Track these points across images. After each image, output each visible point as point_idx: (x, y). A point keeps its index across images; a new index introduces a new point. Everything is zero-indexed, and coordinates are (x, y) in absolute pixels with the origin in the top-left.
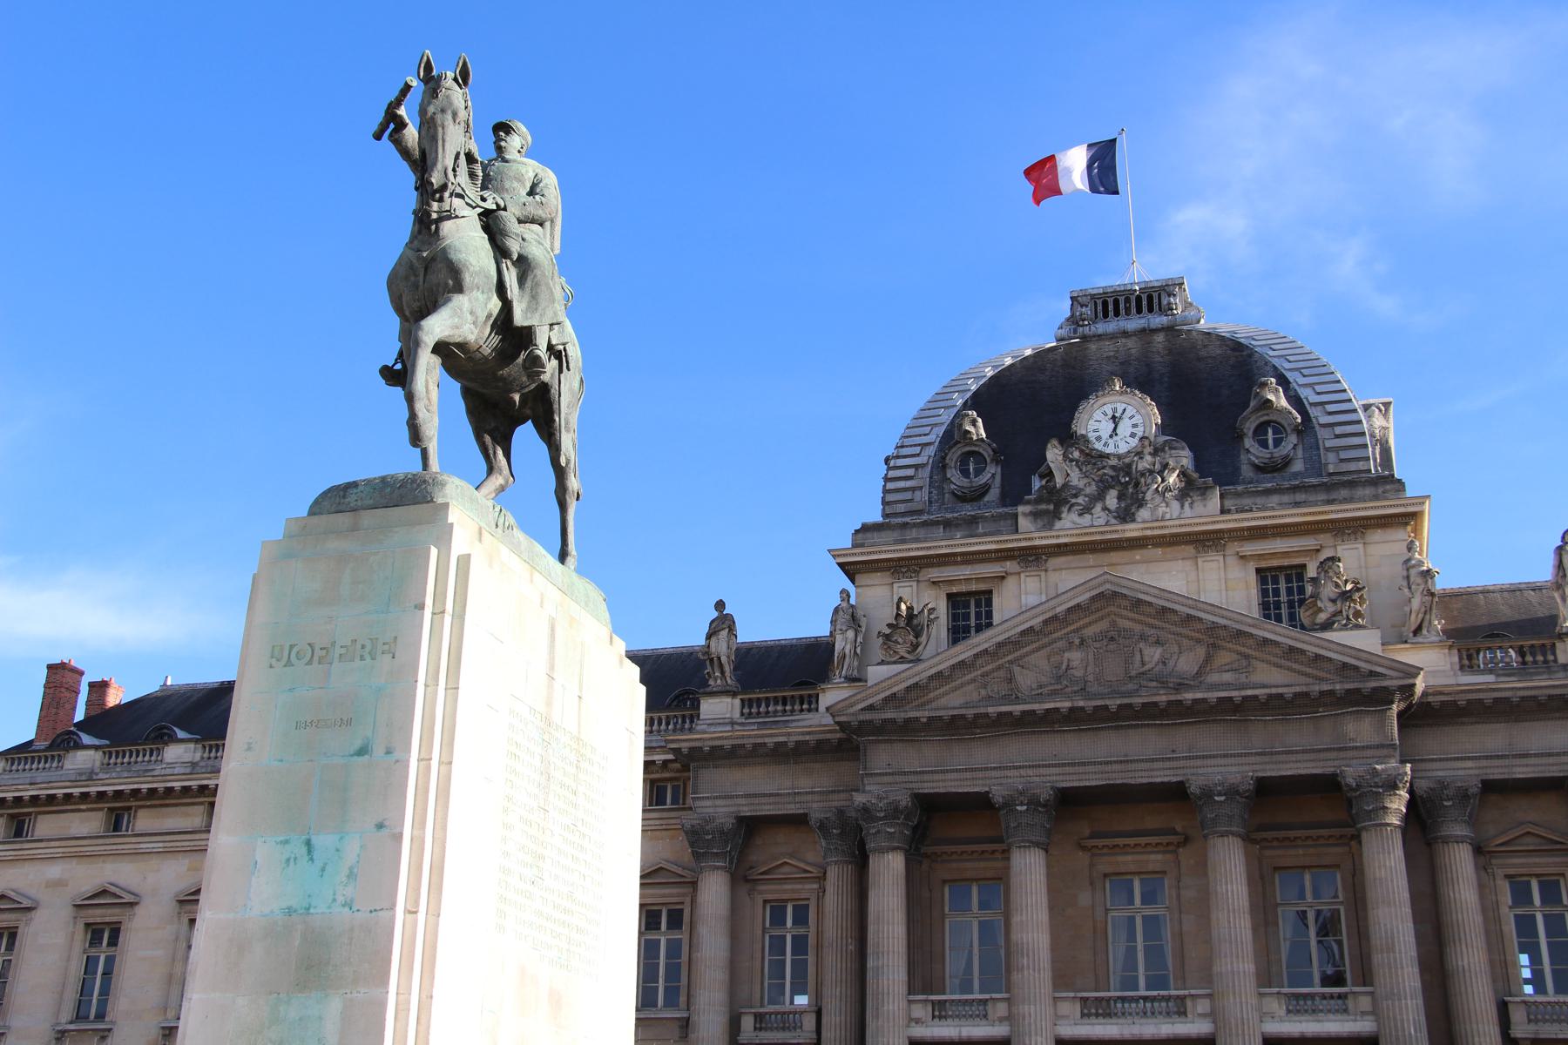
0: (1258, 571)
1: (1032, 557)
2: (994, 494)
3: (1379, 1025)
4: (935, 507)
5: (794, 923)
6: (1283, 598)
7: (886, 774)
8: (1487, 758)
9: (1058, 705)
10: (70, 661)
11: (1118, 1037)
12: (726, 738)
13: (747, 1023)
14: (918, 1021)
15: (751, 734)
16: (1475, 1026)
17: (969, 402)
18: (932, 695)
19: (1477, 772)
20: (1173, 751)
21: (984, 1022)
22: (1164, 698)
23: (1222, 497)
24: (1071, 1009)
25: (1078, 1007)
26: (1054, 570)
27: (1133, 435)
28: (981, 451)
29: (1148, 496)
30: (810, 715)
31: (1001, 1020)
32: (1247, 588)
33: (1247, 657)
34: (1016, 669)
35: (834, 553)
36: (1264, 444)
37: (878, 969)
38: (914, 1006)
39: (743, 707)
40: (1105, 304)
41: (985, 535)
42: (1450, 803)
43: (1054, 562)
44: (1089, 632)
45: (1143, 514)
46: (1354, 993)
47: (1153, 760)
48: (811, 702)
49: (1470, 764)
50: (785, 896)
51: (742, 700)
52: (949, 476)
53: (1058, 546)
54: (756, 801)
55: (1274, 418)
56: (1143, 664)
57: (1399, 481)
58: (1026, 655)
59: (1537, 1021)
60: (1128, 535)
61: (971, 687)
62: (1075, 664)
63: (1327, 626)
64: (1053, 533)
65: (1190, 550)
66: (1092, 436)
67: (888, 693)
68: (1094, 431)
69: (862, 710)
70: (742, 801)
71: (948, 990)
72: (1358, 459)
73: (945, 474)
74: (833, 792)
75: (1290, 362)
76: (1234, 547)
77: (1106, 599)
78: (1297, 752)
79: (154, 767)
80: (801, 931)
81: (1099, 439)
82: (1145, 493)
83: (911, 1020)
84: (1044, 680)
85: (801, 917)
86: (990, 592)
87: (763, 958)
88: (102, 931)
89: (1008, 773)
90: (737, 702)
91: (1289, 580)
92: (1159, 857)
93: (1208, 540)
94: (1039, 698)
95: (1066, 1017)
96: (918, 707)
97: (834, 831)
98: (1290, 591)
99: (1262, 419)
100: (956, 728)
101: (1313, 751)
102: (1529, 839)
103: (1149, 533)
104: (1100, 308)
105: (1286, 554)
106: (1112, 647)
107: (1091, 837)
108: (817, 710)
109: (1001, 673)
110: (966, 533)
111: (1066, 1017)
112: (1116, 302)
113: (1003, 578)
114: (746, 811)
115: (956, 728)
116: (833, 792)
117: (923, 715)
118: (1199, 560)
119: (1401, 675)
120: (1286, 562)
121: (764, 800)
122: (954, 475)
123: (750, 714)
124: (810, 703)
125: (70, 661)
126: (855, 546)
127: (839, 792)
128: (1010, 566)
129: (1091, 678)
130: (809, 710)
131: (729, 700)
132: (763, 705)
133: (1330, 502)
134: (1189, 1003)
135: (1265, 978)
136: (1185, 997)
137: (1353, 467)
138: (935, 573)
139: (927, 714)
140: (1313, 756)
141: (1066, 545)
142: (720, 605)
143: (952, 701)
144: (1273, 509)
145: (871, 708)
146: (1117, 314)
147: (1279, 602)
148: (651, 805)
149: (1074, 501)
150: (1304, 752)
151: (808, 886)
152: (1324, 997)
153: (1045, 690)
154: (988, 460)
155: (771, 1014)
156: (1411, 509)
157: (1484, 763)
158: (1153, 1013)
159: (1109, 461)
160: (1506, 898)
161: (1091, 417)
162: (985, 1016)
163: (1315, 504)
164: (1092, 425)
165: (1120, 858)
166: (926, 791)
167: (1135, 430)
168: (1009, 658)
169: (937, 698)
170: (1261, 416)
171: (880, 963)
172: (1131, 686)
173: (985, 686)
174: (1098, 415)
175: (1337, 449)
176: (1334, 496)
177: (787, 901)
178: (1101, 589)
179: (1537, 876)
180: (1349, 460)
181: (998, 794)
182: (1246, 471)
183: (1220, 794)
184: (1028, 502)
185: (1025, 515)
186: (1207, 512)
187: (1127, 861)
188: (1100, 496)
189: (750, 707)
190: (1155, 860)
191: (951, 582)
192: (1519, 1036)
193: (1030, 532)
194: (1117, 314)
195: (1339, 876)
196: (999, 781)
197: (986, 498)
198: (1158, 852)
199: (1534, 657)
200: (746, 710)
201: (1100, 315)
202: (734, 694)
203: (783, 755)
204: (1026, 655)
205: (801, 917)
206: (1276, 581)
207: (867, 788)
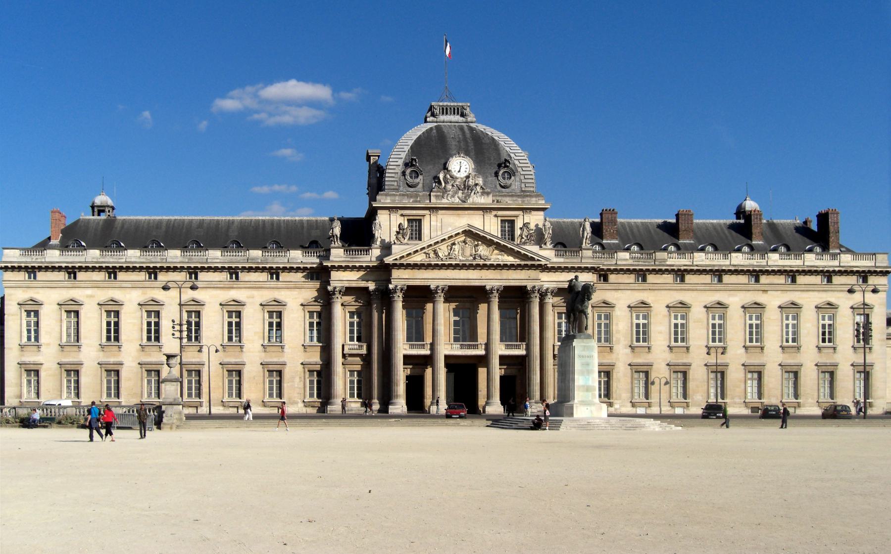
1: (434, 209)
2: (420, 185)
10: (702, 409)
13: (346, 348)
22: (482, 263)
23: (493, 196)
24: (503, 347)
27: (466, 171)
40: (443, 109)
43: (440, 212)
49: (555, 283)
52: (406, 178)
54: (351, 282)
63: (525, 243)
66: (453, 170)
67: (402, 255)
68: (454, 168)
71: (461, 340)
75: (516, 156)
76: (494, 213)
79: (122, 257)
81: (455, 171)
104: (441, 111)
112: (447, 109)
114: (347, 285)
122: (408, 177)
125: (702, 409)
145: (396, 259)
146: (447, 114)
149: (448, 193)
157: (559, 283)
159: (550, 243)
160: (556, 318)
167: (466, 170)
174: (455, 163)
184: (434, 192)
188: (456, 193)
194: (447, 114)
197: (418, 187)
201: (441, 113)
207: (392, 283)
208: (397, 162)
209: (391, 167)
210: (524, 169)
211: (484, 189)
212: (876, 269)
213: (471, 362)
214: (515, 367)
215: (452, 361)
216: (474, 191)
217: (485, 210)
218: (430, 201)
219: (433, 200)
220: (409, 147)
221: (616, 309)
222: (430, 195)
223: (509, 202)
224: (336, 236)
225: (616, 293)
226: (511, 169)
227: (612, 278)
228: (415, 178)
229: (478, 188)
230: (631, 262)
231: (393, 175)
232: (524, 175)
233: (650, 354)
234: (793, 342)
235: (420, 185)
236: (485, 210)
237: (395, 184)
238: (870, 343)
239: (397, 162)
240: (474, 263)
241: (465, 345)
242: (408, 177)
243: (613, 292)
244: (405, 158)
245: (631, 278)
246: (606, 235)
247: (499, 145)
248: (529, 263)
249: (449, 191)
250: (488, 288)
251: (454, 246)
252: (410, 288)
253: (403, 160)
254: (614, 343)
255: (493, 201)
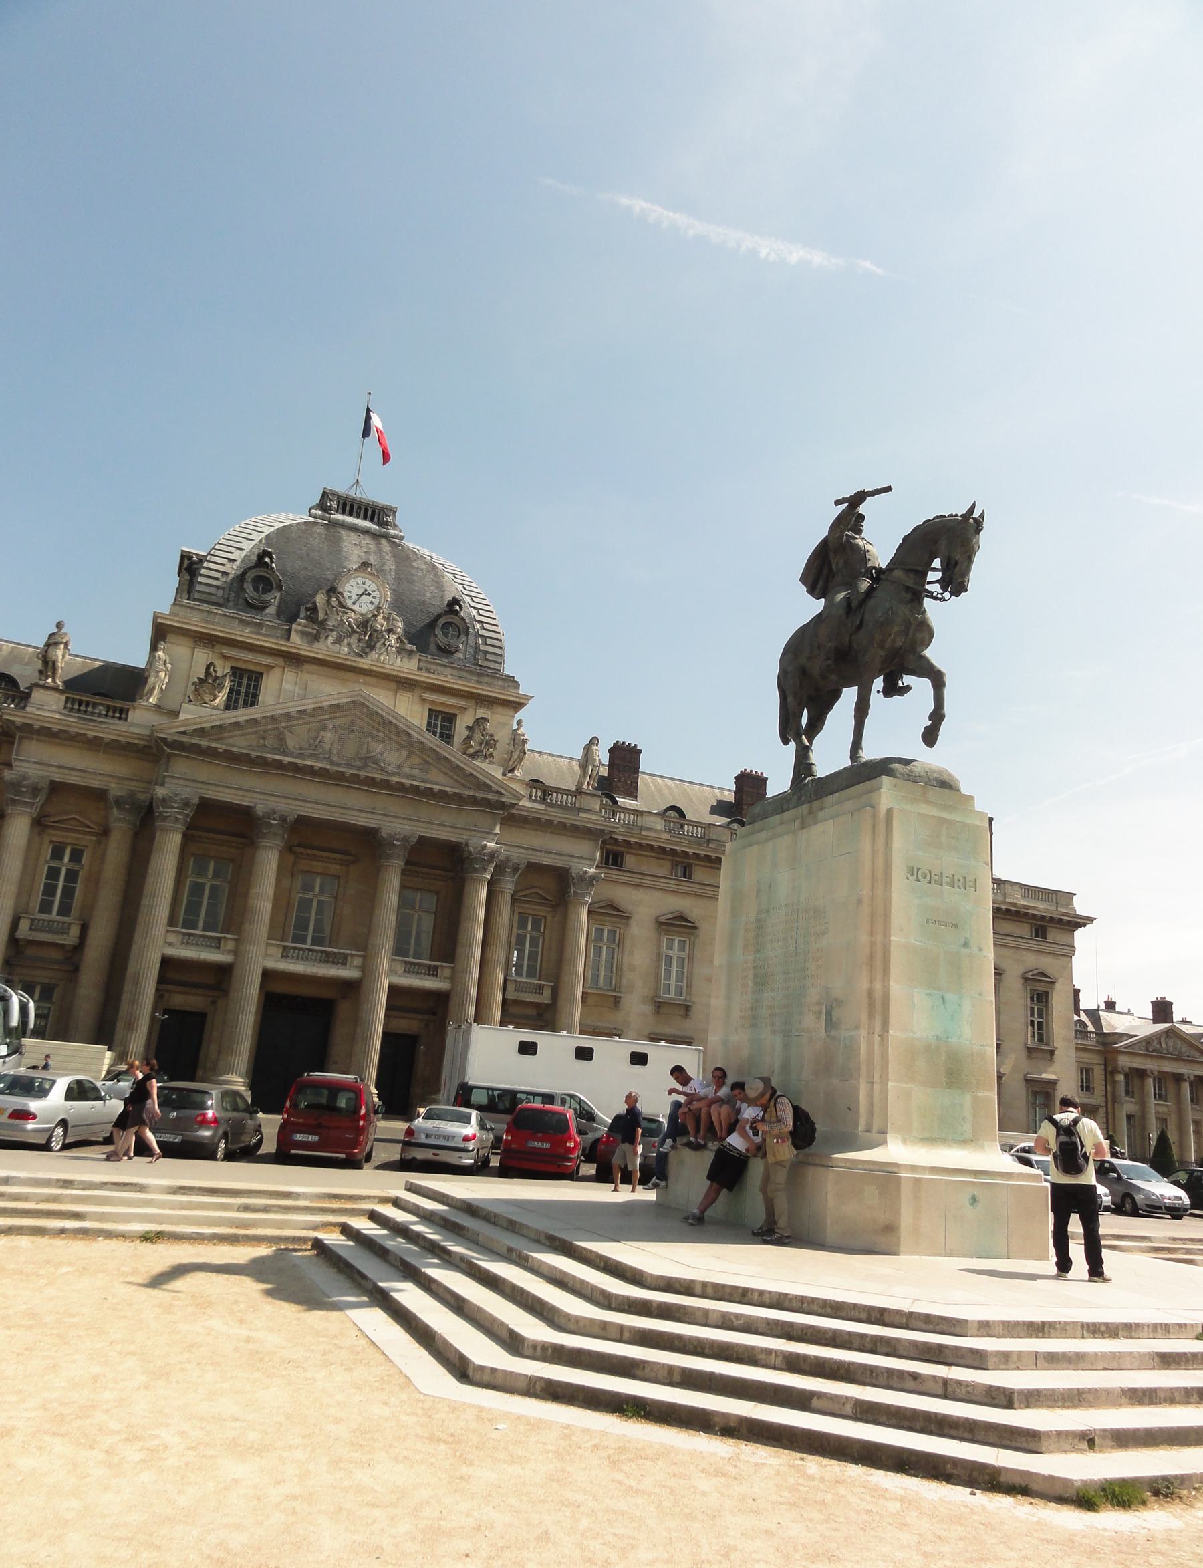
0: (430, 710)
1: (295, 660)
2: (271, 610)
3: (235, 959)
4: (231, 604)
5: (70, 860)
6: (243, 689)
7: (182, 779)
8: (532, 849)
9: (313, 764)
11: (302, 973)
12: (54, 723)
13: (24, 925)
14: (170, 944)
15: (73, 723)
16: (149, 954)
17: (263, 540)
18: (226, 735)
19: (525, 856)
20: (374, 809)
21: (216, 951)
22: (380, 776)
24: (400, 969)
25: (280, 951)
26: (308, 672)
28: (271, 578)
29: (378, 645)
30: (121, 722)
31: (229, 952)
32: (422, 718)
33: (429, 763)
34: (287, 734)
35: (156, 617)
36: (446, 635)
37: (152, 907)
38: (169, 934)
39: (66, 702)
41: (265, 635)
42: (25, 789)
43: (307, 667)
44: (338, 722)
45: (374, 655)
46: (352, 955)
47: (361, 811)
48: (123, 714)
49: (523, 851)
50: (68, 841)
51: (67, 698)
53: (314, 658)
54: (67, 772)
55: (456, 622)
56: (368, 751)
57: (517, 682)
58: (295, 725)
59: (518, 990)
60: (361, 666)
61: (253, 736)
62: (326, 740)
64: (288, 644)
65: (393, 685)
66: (346, 594)
67: (199, 726)
69: (178, 732)
70: (54, 769)
71: (219, 929)
72: (496, 662)
73: (243, 585)
74: (128, 779)
76: (418, 692)
77: (357, 706)
78: (445, 826)
80: (75, 867)
81: (350, 597)
82: (376, 643)
83: (165, 942)
84: (304, 745)
85: (76, 856)
86: (261, 674)
87: (543, 949)
88: (64, 850)
89: (268, 798)
90: (63, 698)
91: (250, 679)
92: (338, 867)
93: (406, 684)
94: (301, 756)
95: (272, 956)
96: (216, 740)
97: (127, 806)
98: (248, 686)
99: (449, 620)
100: (233, 758)
101: (452, 827)
102: (72, 823)
103: (374, 668)
105: (448, 706)
106: (351, 736)
107: (297, 846)
108: (126, 719)
109: (276, 732)
110: (255, 630)
111: (272, 956)
113: (273, 667)
114: (57, 777)
115: (233, 758)
116: (128, 779)
117: (221, 747)
118: (286, 670)
119: (512, 797)
120: (446, 710)
121: (73, 773)
122: (248, 587)
123: (71, 710)
124: (121, 713)
126: (172, 613)
127: (133, 780)
128: (280, 661)
129: (335, 752)
130: (120, 718)
131: (57, 695)
132: (84, 706)
133: (478, 682)
134: (349, 958)
135: (172, 922)
136: (348, 954)
137: (492, 665)
138: (227, 651)
139: (224, 747)
140: (452, 830)
141: (319, 659)
142: (59, 625)
143: (239, 744)
144: (446, 676)
145: (184, 733)
147: (240, 691)
148: (602, 863)
150: (449, 826)
151: (90, 838)
152: (202, 936)
153: (306, 752)
154: (274, 586)
155: (39, 920)
156: (522, 701)
158: (303, 959)
161: (348, 582)
162: (218, 948)
163: (469, 681)
164: (347, 587)
165: (315, 863)
166: (352, 822)
168: (283, 724)
169: (232, 737)
170: (261, 571)
171: (155, 903)
172: (358, 763)
173: (264, 738)
175: (485, 652)
176: (481, 680)
177: (67, 844)
178: (355, 699)
179: (533, 915)
180: (491, 661)
181: (260, 810)
182: (433, 648)
183: (397, 840)
185: (296, 631)
186: (407, 667)
187: (317, 866)
189: (73, 704)
190: (335, 868)
191: (236, 660)
192: (509, 997)
193: (297, 643)
195: (231, 865)
196: (261, 801)
197: (268, 610)
198: (337, 864)
199: (121, 715)
200: (69, 705)
202: (62, 692)
203: (94, 744)
204: (295, 725)
205: (76, 856)
206: (436, 719)
208: (231, 553)
209: (211, 566)
210: (488, 641)
211: (404, 643)
212: (1062, 917)
213: (325, 993)
214: (420, 1017)
215: (281, 988)
216: (383, 640)
217: (404, 684)
218: (288, 639)
219: (295, 638)
220: (263, 535)
221: (633, 923)
222: (289, 631)
223: (446, 677)
224: (54, 663)
225: (634, 892)
226: (463, 619)
227: (630, 861)
228: (263, 593)
229: (393, 639)
230: (666, 836)
231: (218, 575)
232: (481, 622)
233: (688, 1020)
234: (528, 976)
235: (271, 610)
236: (404, 684)
237: (220, 593)
238: (1051, 1044)
239: (231, 553)
240: (363, 774)
241: (315, 951)
242: (248, 587)
243: (629, 890)
244: (251, 551)
245: (663, 868)
246: (616, 786)
247: (443, 577)
248: (479, 795)
249: (332, 630)
250: (384, 834)
251: (322, 733)
252: (207, 808)
253: (244, 553)
254: (622, 990)
255: (420, 669)
